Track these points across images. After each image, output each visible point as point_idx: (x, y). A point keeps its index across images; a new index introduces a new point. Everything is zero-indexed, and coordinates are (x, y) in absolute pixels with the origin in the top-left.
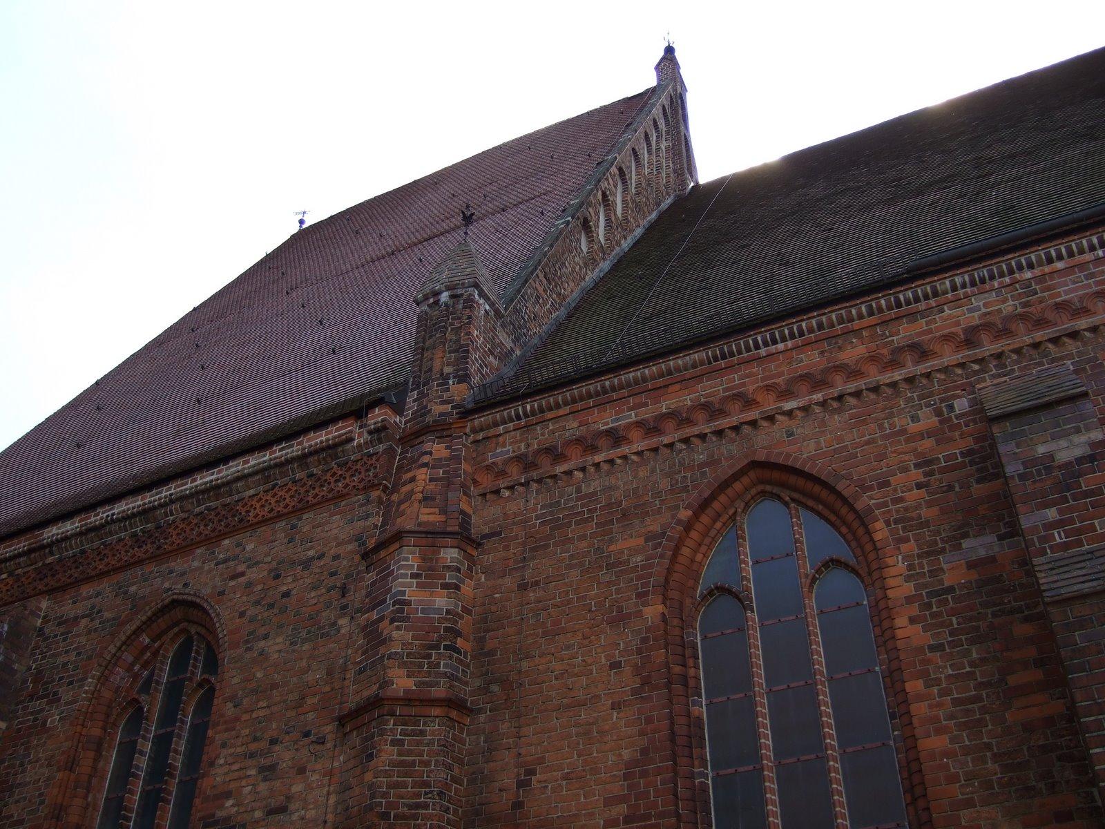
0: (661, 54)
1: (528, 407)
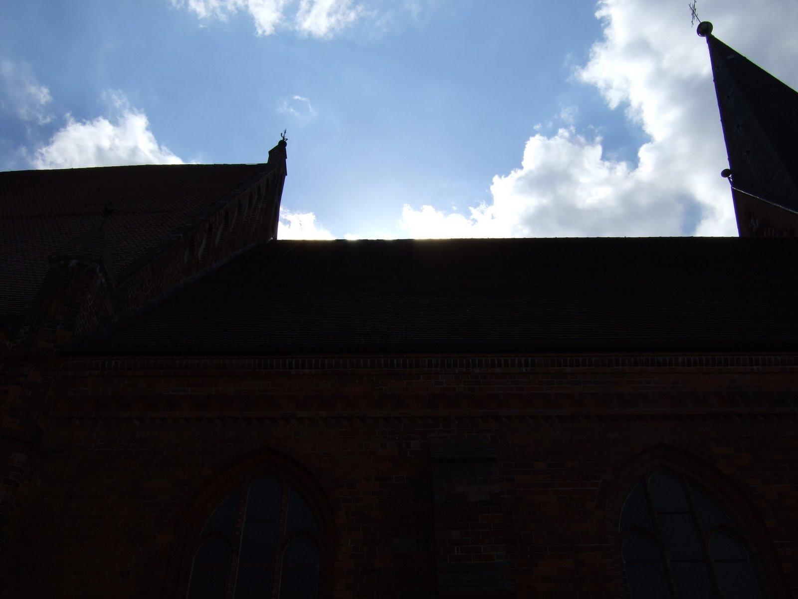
0: (276, 144)
1: (113, 363)
